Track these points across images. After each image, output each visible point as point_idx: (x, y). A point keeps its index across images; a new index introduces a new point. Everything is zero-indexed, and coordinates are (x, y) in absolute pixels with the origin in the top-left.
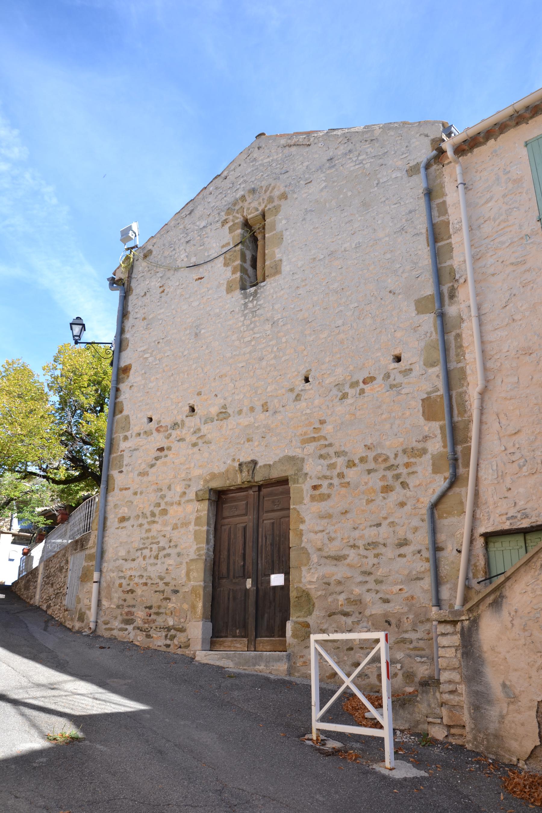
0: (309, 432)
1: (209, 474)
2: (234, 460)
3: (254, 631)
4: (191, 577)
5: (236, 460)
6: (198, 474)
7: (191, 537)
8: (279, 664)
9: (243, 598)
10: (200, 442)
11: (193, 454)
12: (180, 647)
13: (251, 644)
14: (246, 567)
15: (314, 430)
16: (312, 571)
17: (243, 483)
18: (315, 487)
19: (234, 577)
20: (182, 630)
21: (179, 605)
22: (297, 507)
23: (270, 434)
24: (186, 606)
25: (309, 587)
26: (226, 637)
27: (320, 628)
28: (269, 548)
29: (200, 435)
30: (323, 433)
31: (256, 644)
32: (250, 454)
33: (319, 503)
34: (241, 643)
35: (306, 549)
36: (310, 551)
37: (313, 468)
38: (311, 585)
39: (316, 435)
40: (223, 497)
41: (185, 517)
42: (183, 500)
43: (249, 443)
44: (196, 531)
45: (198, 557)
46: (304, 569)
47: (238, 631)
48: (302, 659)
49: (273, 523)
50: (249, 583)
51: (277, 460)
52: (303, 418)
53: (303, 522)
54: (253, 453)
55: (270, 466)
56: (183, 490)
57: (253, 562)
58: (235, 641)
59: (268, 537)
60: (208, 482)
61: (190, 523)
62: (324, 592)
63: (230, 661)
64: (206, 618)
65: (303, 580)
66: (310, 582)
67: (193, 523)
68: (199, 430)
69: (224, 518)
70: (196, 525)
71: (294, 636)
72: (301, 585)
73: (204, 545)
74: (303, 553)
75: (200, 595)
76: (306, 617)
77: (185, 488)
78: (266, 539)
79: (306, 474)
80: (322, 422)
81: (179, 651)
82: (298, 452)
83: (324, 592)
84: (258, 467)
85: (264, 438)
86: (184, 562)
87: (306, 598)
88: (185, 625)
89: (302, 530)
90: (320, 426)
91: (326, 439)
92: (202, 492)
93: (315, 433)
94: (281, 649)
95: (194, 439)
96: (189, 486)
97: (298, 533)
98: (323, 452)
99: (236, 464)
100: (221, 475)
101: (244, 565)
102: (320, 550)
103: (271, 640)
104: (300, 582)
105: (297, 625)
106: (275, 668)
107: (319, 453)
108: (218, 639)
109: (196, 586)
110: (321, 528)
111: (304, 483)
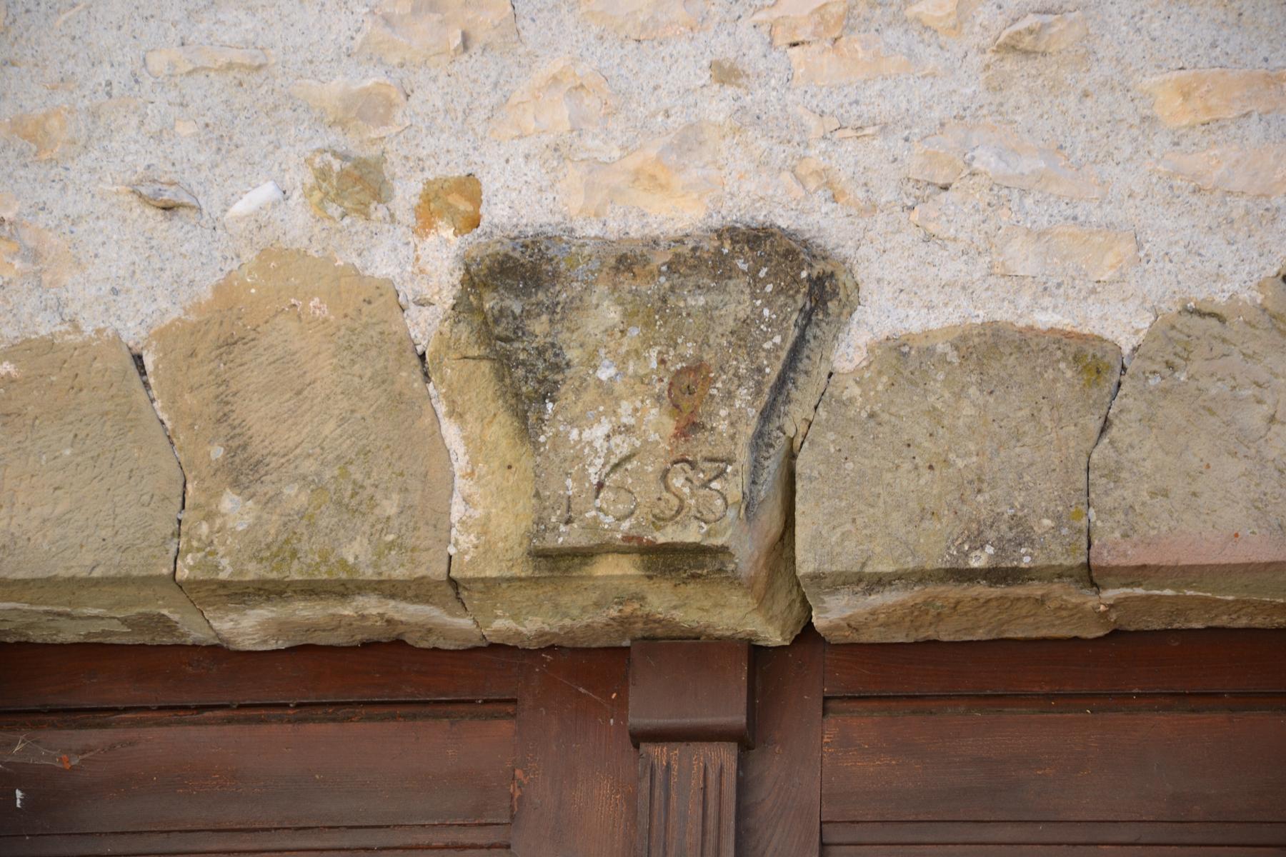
55: (1093, 362)
84: (850, 348)
99: (424, 268)
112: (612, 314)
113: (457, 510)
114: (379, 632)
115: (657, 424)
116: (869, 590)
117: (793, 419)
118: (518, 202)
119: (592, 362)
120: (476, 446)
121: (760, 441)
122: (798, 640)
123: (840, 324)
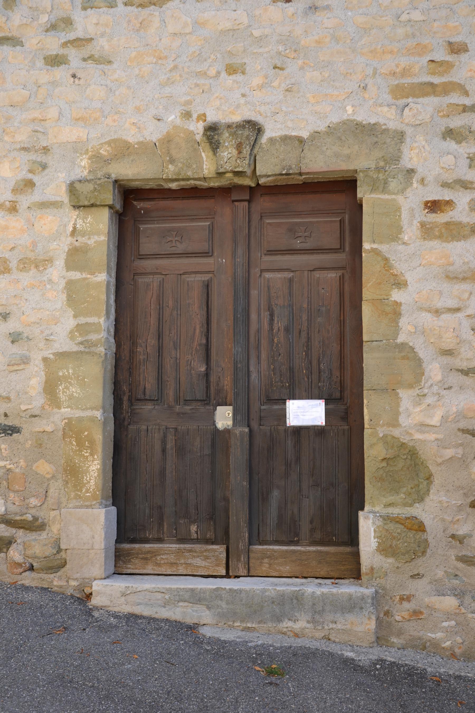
0: (416, 69)
1: (109, 143)
2: (187, 115)
3: (246, 530)
4: (62, 397)
5: (195, 116)
6: (74, 138)
7: (58, 299)
8: (351, 617)
9: (207, 451)
10: (74, 55)
11: (54, 84)
12: (31, 568)
13: (239, 560)
14: (213, 378)
15: (433, 65)
16: (430, 400)
17: (220, 174)
18: (434, 206)
19: (177, 400)
20: (35, 526)
21: (22, 463)
22: (384, 248)
23: (300, 62)
24: (44, 468)
25: (418, 436)
26: (160, 540)
27: (451, 531)
28: (280, 338)
29: (72, 36)
30: (458, 76)
31: (252, 561)
32: (238, 106)
33: (444, 244)
34: (207, 558)
35: (412, 349)
36: (421, 354)
37: (430, 159)
38: (422, 432)
39: (436, 80)
40: (139, 205)
41: (34, 244)
42: (25, 201)
43: (233, 77)
44: (70, 284)
45: (82, 348)
46: (406, 396)
47: (194, 528)
48: (406, 605)
49: (291, 280)
50: (224, 417)
51: (322, 127)
52: (400, 31)
53: (400, 284)
54: (247, 103)
55: (301, 140)
56: (24, 174)
57: (236, 368)
58: (190, 551)
59: (277, 312)
60: (107, 162)
61: (49, 261)
62: (460, 451)
63: (204, 608)
64: (107, 499)
65: (403, 420)
66: (423, 425)
67: (60, 263)
68: (68, 22)
69: (142, 257)
70: (69, 266)
71: (385, 549)
72: (396, 432)
73: (102, 320)
74: (403, 358)
75: (92, 442)
76: (411, 505)
77: (30, 171)
78: (272, 315)
79: (411, 172)
80: (457, 49)
81: (28, 579)
82: (387, 117)
83: (460, 451)
84: (264, 139)
85: (282, 69)
86: (37, 358)
87: (409, 462)
88: (41, 514)
89: (398, 304)
90: (449, 58)
91: (466, 94)
92: (91, 187)
93: (433, 74)
94: (323, 574)
95: (53, 44)
96: (44, 167)
97: (388, 309)
98: (456, 122)
99: (198, 128)
100: (147, 149)
101: (207, 375)
102: (448, 353)
103: (294, 552)
104: (395, 423)
105: (391, 526)
106: (339, 626)
107: (443, 124)
108: (137, 546)
109: (80, 420)
110: (451, 303)
111: (403, 191)
112: (227, 135)
113: (205, 167)
114: (194, 186)
115: (235, 152)
116: (268, 177)
117: (255, 151)
118: (212, 117)
119: (224, 142)
120: (207, 157)
121: (251, 154)
122: (257, 186)
123: (262, 135)
